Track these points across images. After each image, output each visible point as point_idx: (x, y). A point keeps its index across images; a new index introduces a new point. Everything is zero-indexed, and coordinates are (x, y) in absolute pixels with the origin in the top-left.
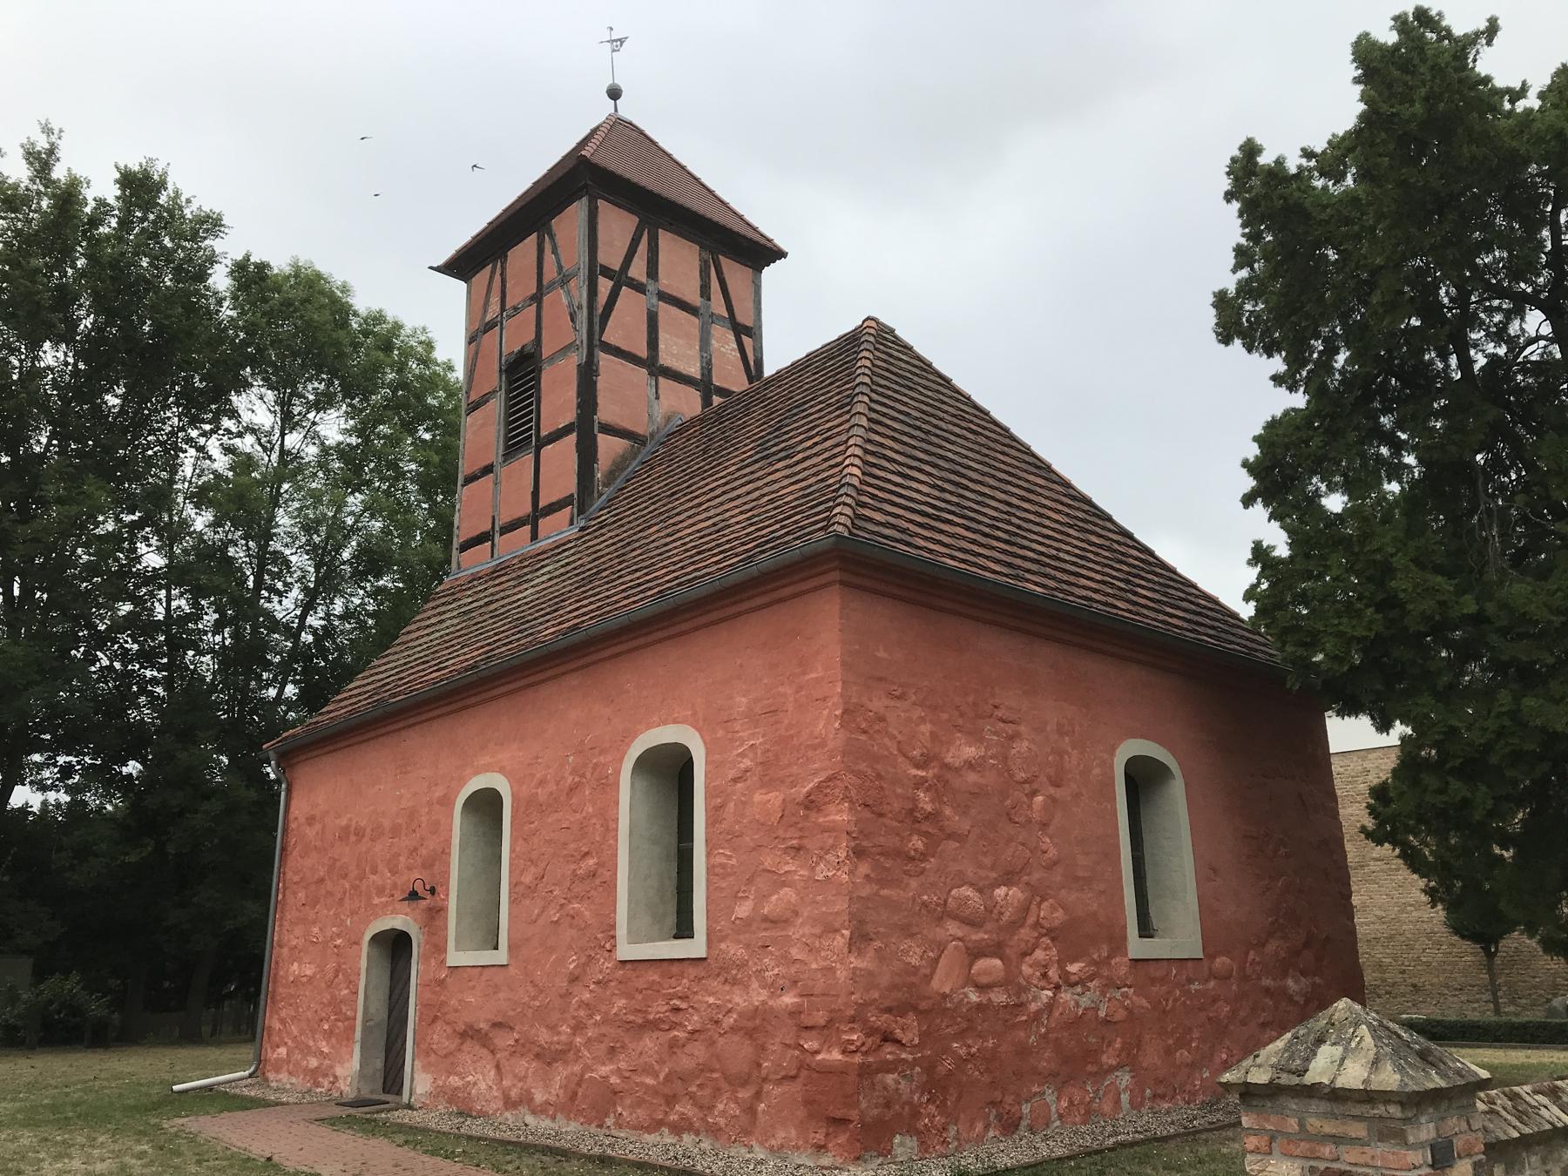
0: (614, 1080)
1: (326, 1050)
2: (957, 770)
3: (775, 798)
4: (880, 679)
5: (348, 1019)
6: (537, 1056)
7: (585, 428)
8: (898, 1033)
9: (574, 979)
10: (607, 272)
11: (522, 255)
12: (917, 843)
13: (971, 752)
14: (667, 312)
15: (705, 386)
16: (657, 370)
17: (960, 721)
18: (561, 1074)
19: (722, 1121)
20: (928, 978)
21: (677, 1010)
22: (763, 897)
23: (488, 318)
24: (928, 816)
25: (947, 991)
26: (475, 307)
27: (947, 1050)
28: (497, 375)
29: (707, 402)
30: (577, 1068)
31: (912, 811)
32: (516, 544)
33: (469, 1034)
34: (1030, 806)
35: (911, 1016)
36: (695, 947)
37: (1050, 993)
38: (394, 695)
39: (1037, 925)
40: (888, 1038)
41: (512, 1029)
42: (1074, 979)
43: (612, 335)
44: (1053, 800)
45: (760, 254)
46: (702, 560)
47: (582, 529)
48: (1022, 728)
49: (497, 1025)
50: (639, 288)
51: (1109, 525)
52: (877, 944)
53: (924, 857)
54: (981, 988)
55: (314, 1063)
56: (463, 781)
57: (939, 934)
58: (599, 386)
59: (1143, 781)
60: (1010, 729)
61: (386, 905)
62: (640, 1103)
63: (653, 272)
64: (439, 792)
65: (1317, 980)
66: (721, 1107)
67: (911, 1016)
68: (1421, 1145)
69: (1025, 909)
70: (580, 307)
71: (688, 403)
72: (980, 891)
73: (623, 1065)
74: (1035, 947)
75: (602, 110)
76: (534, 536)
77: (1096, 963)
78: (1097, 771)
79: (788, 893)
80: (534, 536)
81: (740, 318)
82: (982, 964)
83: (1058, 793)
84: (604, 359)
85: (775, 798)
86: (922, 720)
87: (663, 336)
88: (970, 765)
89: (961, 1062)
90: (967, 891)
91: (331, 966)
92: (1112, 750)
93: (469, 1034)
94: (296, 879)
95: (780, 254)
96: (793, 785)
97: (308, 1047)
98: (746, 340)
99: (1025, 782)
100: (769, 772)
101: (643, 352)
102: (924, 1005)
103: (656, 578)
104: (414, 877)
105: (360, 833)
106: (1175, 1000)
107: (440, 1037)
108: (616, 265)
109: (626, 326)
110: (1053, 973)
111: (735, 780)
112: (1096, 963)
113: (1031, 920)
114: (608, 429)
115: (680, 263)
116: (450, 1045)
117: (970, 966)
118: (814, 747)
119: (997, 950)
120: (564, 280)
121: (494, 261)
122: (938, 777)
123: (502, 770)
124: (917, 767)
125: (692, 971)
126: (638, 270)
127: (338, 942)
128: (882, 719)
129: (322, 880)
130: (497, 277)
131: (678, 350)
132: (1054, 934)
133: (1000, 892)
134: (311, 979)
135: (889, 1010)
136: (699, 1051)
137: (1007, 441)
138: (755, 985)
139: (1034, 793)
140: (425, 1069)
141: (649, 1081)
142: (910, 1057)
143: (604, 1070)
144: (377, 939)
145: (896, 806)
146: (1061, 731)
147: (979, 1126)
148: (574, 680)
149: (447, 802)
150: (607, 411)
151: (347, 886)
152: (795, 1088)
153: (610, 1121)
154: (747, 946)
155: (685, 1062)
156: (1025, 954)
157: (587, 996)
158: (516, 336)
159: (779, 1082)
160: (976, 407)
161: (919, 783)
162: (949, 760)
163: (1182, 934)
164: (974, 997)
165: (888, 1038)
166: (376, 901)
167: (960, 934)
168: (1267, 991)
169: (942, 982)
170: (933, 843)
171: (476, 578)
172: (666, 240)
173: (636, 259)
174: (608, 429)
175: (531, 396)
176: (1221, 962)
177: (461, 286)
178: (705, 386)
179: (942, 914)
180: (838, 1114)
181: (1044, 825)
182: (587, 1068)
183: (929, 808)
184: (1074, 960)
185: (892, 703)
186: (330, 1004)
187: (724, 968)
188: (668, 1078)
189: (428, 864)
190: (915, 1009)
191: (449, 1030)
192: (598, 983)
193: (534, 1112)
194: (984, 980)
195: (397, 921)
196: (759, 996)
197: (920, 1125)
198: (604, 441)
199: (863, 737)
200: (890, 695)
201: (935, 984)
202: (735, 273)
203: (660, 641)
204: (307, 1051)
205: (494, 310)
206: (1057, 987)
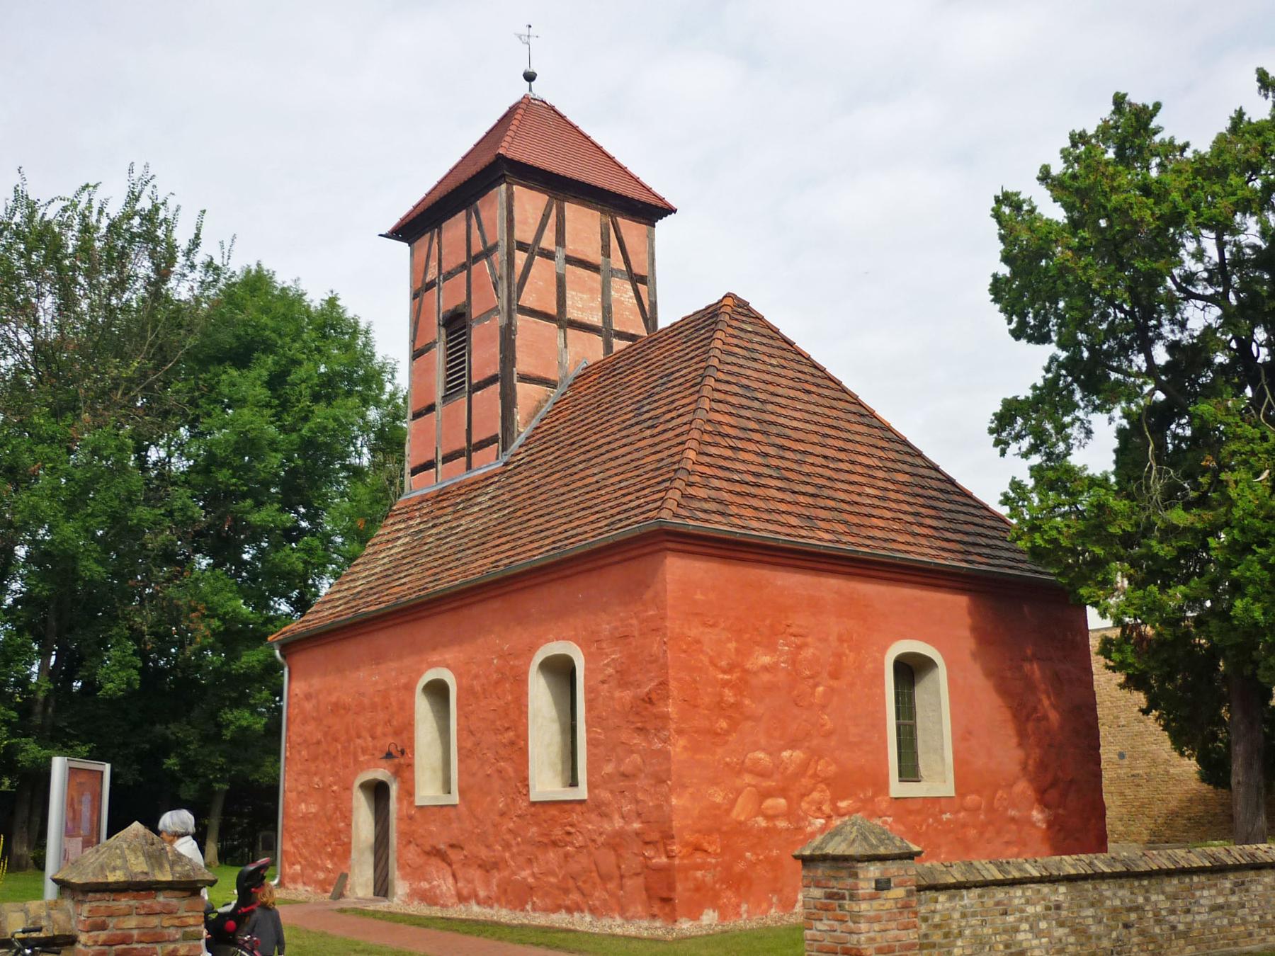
0: (531, 880)
1: (330, 866)
2: (755, 673)
3: (627, 695)
4: (697, 614)
5: (344, 844)
6: (480, 866)
7: (505, 379)
8: (706, 845)
9: (502, 814)
10: (522, 246)
11: (455, 228)
12: (724, 724)
13: (766, 660)
14: (573, 272)
15: (606, 332)
16: (562, 320)
17: (759, 639)
18: (496, 877)
19: (597, 903)
20: (728, 811)
21: (569, 833)
22: (620, 761)
23: (428, 279)
24: (731, 706)
25: (742, 818)
26: (418, 270)
27: (741, 857)
28: (436, 329)
29: (608, 347)
30: (506, 873)
31: (719, 703)
32: (454, 474)
33: (437, 853)
34: (813, 694)
35: (716, 836)
36: (582, 792)
37: (823, 821)
38: (367, 604)
39: (815, 775)
40: (698, 848)
41: (462, 849)
42: (842, 811)
43: (528, 300)
44: (831, 690)
45: (651, 211)
46: (584, 517)
47: (506, 464)
48: (809, 640)
49: (452, 846)
50: (549, 255)
51: (919, 461)
52: (691, 790)
53: (727, 732)
54: (768, 818)
55: (321, 875)
56: (420, 674)
57: (738, 783)
58: (517, 343)
59: (910, 671)
60: (798, 641)
61: (368, 761)
62: (547, 894)
63: (560, 240)
64: (403, 680)
65: (1061, 811)
66: (597, 894)
67: (716, 836)
68: (869, 880)
69: (805, 766)
70: (501, 278)
71: (589, 350)
72: (770, 754)
73: (536, 870)
74: (812, 790)
75: (520, 89)
76: (469, 467)
77: (862, 801)
78: (870, 666)
79: (636, 758)
80: (469, 467)
81: (636, 269)
82: (769, 802)
83: (834, 683)
84: (520, 320)
85: (627, 695)
86: (729, 640)
87: (570, 294)
88: (766, 668)
89: (752, 865)
90: (761, 755)
91: (331, 805)
92: (883, 650)
93: (437, 853)
94: (299, 740)
95: (670, 211)
96: (639, 686)
97: (317, 865)
98: (641, 287)
99: (809, 677)
100: (623, 678)
101: (553, 310)
102: (725, 828)
103: (553, 527)
104: (388, 742)
105: (347, 709)
106: (928, 826)
107: (412, 854)
108: (529, 238)
109: (538, 293)
110: (826, 808)
111: (603, 682)
112: (862, 801)
113: (810, 772)
114: (525, 378)
115: (583, 224)
116: (420, 860)
117: (761, 803)
118: (651, 662)
119: (783, 792)
120: (488, 252)
121: (432, 230)
122: (741, 679)
123: (448, 667)
124: (724, 672)
125: (578, 808)
126: (548, 242)
127: (335, 788)
128: (698, 642)
129: (319, 743)
130: (436, 240)
131: (583, 306)
132: (827, 781)
133: (786, 754)
134: (315, 815)
135: (699, 831)
136: (584, 860)
137: (839, 395)
138: (616, 817)
139: (816, 685)
140: (404, 877)
141: (553, 880)
142: (713, 861)
143: (525, 873)
144: (365, 786)
145: (707, 700)
146: (841, 639)
147: (764, 906)
148: (496, 604)
149: (409, 688)
150: (523, 364)
151: (339, 747)
152: (641, 880)
153: (529, 907)
154: (612, 792)
155: (574, 867)
156: (803, 796)
157: (511, 825)
158: (448, 298)
159: (630, 877)
160: (816, 366)
161: (725, 684)
162: (748, 666)
163: (938, 780)
164: (762, 822)
165: (698, 848)
166: (362, 758)
167: (753, 782)
168: (1013, 819)
169: (740, 812)
170: (734, 725)
171: (424, 500)
172: (571, 209)
173: (546, 232)
174: (525, 378)
175: (463, 348)
176: (971, 799)
177: (404, 247)
178: (606, 332)
179: (740, 770)
180: (665, 895)
181: (823, 707)
182: (514, 873)
183: (732, 700)
184: (843, 798)
185: (707, 630)
186: (331, 833)
187: (598, 806)
188: (564, 878)
189: (397, 733)
190: (719, 830)
191: (419, 850)
192: (519, 816)
193: (478, 903)
194: (770, 812)
195: (381, 774)
196: (618, 823)
197: (721, 902)
198: (522, 389)
199: (683, 655)
200: (704, 624)
201: (734, 814)
202: (631, 229)
203: (552, 580)
204: (316, 867)
205: (432, 274)
206: (829, 817)
